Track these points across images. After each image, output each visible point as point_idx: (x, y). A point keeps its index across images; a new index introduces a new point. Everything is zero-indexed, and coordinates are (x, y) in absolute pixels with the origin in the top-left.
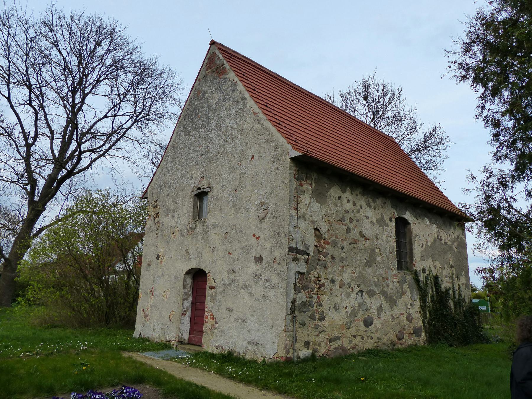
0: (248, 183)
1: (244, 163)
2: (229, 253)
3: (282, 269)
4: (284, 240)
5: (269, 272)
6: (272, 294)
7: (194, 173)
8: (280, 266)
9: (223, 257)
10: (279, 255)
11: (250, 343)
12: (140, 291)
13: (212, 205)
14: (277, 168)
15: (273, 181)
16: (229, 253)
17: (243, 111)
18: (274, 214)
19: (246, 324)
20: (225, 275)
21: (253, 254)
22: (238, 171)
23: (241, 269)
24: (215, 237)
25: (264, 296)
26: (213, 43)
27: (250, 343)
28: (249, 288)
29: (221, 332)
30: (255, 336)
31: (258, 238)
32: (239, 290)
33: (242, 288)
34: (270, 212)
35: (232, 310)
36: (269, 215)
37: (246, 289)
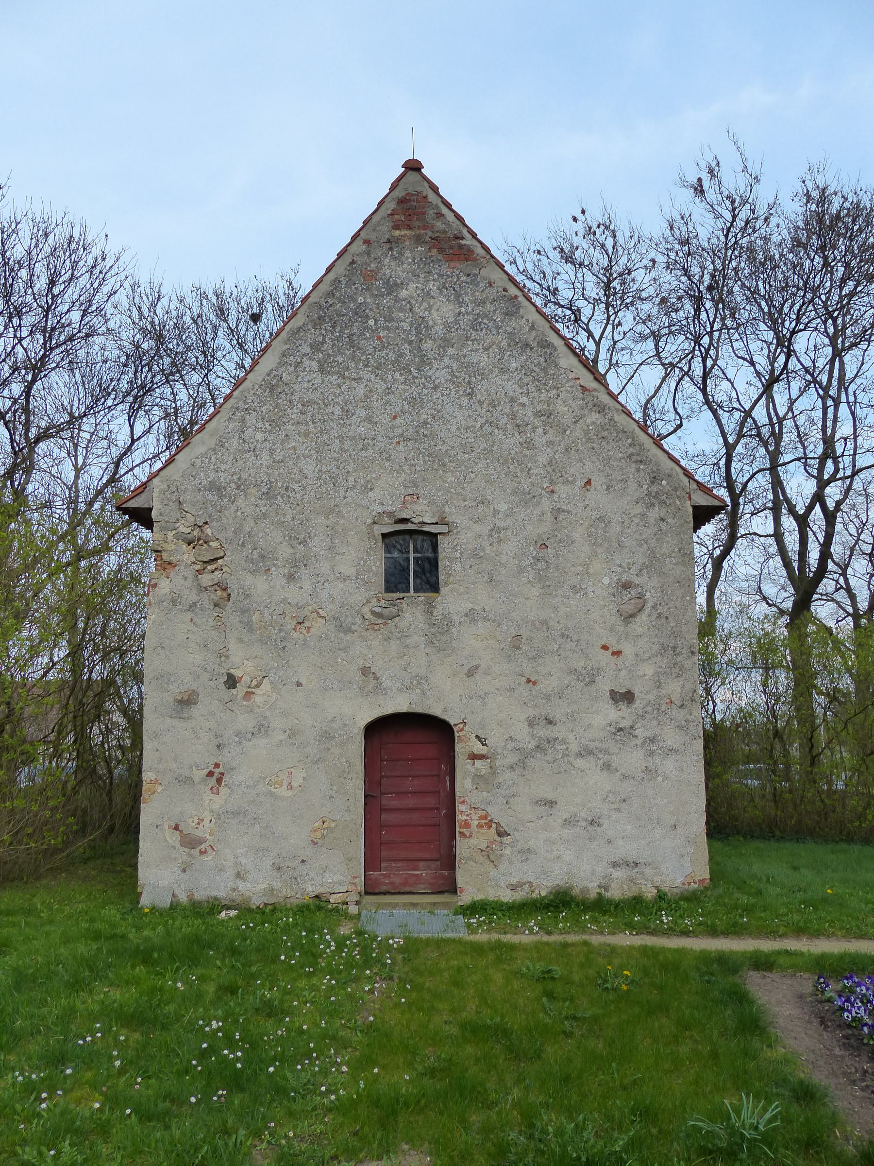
0: (578, 534)
1: (562, 490)
2: (529, 681)
3: (690, 718)
4: (689, 662)
5: (655, 723)
6: (669, 765)
7: (378, 478)
8: (682, 712)
9: (511, 690)
10: (679, 690)
11: (615, 865)
12: (147, 776)
13: (457, 567)
14: (662, 519)
15: (653, 543)
16: (529, 681)
17: (545, 370)
18: (660, 609)
19: (599, 829)
20: (521, 731)
21: (605, 685)
22: (546, 504)
23: (572, 717)
24: (472, 641)
25: (647, 770)
26: (413, 167)
27: (615, 865)
28: (601, 756)
29: (522, 852)
30: (626, 849)
31: (617, 653)
32: (571, 759)
33: (579, 755)
34: (649, 604)
35: (552, 803)
36: (647, 610)
37: (591, 758)
